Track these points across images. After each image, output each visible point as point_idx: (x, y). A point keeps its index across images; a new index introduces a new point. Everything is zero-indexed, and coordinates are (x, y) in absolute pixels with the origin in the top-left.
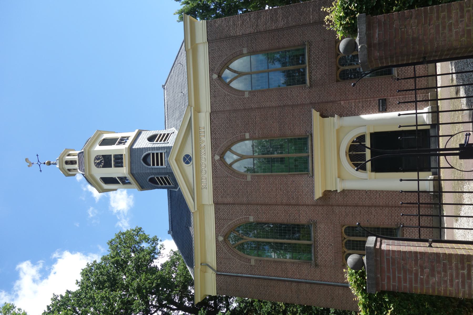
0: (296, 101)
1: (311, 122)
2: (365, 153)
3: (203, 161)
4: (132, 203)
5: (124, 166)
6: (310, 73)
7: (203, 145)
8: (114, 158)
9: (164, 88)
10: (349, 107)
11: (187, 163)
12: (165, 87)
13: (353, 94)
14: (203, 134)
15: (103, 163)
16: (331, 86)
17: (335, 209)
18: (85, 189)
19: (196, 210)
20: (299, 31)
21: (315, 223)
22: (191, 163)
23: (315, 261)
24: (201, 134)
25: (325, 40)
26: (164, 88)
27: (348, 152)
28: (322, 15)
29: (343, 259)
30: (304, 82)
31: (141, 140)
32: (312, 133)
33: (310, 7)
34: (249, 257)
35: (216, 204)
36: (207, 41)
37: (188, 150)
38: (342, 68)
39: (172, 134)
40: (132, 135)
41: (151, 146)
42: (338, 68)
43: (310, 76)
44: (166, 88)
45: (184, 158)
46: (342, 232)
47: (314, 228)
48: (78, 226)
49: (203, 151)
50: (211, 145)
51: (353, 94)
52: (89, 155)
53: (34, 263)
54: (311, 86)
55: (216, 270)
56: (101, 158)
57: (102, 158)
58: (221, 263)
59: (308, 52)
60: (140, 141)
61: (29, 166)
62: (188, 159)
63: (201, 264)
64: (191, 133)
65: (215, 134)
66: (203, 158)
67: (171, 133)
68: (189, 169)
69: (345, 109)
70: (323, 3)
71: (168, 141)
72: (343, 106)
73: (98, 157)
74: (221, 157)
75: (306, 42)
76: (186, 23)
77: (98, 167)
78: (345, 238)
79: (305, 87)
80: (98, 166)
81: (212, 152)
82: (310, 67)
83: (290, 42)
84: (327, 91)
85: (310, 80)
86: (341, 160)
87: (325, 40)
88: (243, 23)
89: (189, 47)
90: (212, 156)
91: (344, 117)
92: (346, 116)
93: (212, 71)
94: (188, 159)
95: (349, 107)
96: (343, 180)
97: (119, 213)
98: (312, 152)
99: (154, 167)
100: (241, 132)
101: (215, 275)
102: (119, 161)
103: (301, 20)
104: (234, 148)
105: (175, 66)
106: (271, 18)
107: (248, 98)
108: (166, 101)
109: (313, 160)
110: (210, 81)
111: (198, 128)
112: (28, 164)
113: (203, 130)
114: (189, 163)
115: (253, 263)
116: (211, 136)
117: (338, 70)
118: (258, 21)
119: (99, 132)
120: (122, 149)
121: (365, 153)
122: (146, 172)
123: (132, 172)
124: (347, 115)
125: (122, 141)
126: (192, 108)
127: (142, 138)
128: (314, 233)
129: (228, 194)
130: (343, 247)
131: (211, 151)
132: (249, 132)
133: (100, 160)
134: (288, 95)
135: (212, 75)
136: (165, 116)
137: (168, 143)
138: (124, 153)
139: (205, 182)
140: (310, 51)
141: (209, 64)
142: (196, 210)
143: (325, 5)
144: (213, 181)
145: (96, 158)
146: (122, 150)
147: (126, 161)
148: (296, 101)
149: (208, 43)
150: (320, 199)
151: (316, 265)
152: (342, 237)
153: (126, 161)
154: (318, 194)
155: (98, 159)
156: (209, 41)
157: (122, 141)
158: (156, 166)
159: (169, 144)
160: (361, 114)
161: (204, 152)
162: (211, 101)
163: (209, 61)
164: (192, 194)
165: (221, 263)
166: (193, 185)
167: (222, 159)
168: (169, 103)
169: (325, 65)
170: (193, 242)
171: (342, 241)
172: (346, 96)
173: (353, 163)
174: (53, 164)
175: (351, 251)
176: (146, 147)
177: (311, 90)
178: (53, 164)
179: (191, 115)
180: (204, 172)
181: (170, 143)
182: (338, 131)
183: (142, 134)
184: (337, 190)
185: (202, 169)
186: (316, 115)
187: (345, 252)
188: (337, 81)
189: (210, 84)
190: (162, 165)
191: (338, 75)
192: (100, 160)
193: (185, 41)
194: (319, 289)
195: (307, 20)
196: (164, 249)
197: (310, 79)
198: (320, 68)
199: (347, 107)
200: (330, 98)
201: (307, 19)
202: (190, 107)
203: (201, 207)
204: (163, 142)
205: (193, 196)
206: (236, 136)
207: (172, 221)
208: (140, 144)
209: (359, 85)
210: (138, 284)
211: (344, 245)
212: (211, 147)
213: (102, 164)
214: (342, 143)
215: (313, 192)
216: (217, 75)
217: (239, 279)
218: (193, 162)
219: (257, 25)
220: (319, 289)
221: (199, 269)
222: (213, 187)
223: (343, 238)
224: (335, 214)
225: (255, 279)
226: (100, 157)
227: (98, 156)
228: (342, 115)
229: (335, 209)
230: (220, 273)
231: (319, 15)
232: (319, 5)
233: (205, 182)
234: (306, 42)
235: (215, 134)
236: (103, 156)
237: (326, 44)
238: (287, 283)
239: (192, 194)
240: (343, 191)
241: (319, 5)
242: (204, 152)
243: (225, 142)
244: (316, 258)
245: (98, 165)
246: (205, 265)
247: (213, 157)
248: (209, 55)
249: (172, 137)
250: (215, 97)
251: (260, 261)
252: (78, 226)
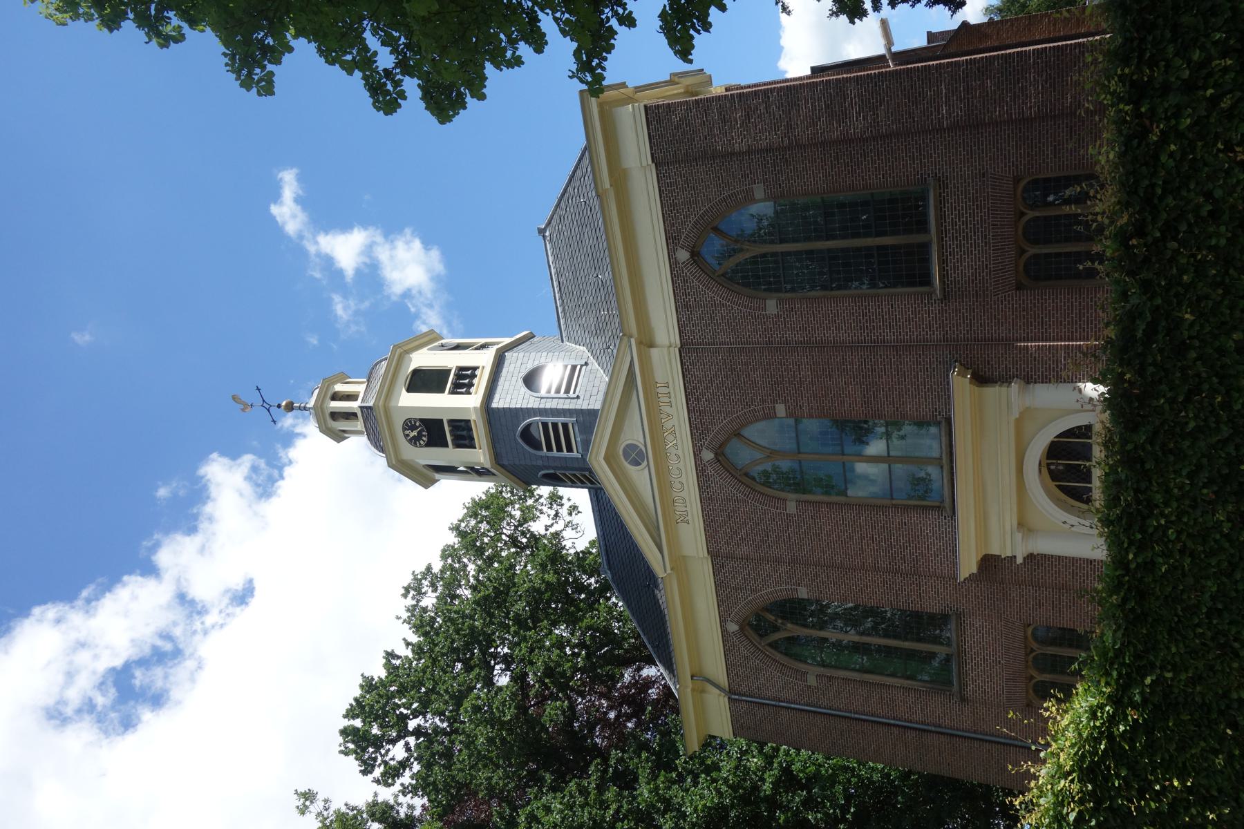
0: (907, 332)
1: (948, 389)
2: (1089, 485)
3: (672, 460)
4: (440, 268)
5: (477, 446)
6: (942, 262)
7: (668, 425)
8: (451, 435)
9: (544, 237)
10: (1050, 359)
11: (636, 463)
12: (547, 234)
13: (1061, 325)
14: (667, 400)
15: (425, 436)
16: (1002, 301)
17: (1010, 590)
18: (312, 249)
19: (669, 571)
20: (909, 144)
21: (959, 616)
22: (645, 463)
23: (961, 692)
24: (660, 390)
25: (984, 174)
26: (544, 237)
27: (1045, 462)
28: (976, 106)
29: (1027, 692)
30: (926, 280)
31: (507, 383)
32: (950, 415)
33: (941, 81)
34: (802, 667)
35: (716, 556)
36: (653, 161)
37: (635, 434)
38: (1032, 251)
39: (584, 368)
40: (483, 360)
41: (536, 406)
42: (1023, 251)
43: (942, 269)
44: (548, 238)
45: (624, 450)
46: (1026, 638)
47: (957, 626)
48: (315, 342)
49: (671, 438)
50: (691, 427)
51: (1061, 325)
52: (394, 445)
53: (233, 454)
54: (946, 296)
55: (727, 689)
56: (418, 424)
57: (420, 426)
58: (737, 675)
59: (936, 207)
60: (506, 387)
61: (243, 410)
62: (635, 456)
63: (692, 677)
64: (635, 393)
65: (698, 400)
66: (673, 454)
67: (582, 366)
68: (641, 477)
69: (1039, 364)
70: (979, 72)
71: (577, 393)
72: (1035, 357)
73: (410, 422)
74: (716, 454)
75: (929, 176)
76: (590, 126)
77: (415, 445)
78: (1032, 650)
79: (930, 294)
80: (415, 444)
81: (693, 442)
82: (941, 247)
83: (883, 175)
84: (991, 312)
85: (944, 282)
86: (1027, 487)
87: (984, 174)
88: (748, 116)
89: (607, 185)
90: (694, 452)
91: (1035, 383)
92: (1043, 383)
93: (672, 239)
94: (635, 456)
95: (1050, 359)
96: (1030, 530)
97: (407, 294)
98: (951, 461)
99: (550, 454)
100: (763, 401)
101: (726, 699)
102: (462, 433)
103: (914, 118)
104: (749, 432)
105: (567, 195)
106: (827, 106)
107: (777, 316)
108: (553, 271)
109: (953, 480)
110: (670, 266)
111: (650, 385)
112: (242, 407)
113: (665, 390)
114: (640, 464)
115: (812, 681)
116: (687, 403)
117: (1020, 257)
118: (790, 114)
119: (399, 351)
120: (468, 403)
121: (1089, 485)
122: (534, 463)
123: (497, 457)
124: (1044, 380)
125: (464, 380)
126: (633, 341)
127: (510, 375)
128: (957, 636)
129: (742, 539)
130: (1027, 667)
131: (692, 439)
132: (785, 402)
133: (417, 431)
134: (883, 316)
135: (675, 251)
136: (549, 266)
137: (578, 397)
138: (473, 417)
139: (684, 509)
140: (940, 202)
141: (664, 222)
142: (669, 571)
143: (985, 77)
144: (702, 506)
145: (407, 425)
146: (466, 410)
147: (480, 433)
148: (907, 332)
149: (656, 165)
150: (971, 578)
151: (963, 700)
152: (1026, 647)
153: (480, 433)
154: (968, 566)
155: (413, 428)
156: (658, 162)
157: (464, 380)
158: (555, 453)
159: (580, 401)
160: (1084, 379)
161: (675, 442)
162: (678, 317)
163: (663, 214)
164: (655, 535)
165: (737, 675)
166: (655, 516)
167: (720, 459)
168: (563, 279)
169: (986, 242)
170: (667, 618)
171: (1027, 655)
172: (1042, 328)
173: (1057, 486)
174: (299, 408)
175: (1048, 676)
176: (524, 406)
177: (946, 306)
178: (299, 408)
179: (632, 357)
180: (677, 485)
181: (582, 397)
182: (1019, 423)
183: (507, 363)
184: (1015, 557)
185: (673, 479)
186: (960, 383)
187: (1032, 677)
188: (1019, 287)
189: (672, 274)
190: (570, 449)
191: (1021, 268)
192: (417, 431)
193: (588, 149)
194: (971, 748)
195: (932, 119)
196: (579, 512)
197: (942, 278)
198: (972, 251)
199: (1045, 359)
200: (999, 329)
201: (932, 115)
202: (625, 339)
203: (680, 564)
204: (565, 396)
205: (658, 541)
206: (752, 408)
207: (607, 551)
208: (509, 397)
209: (1080, 302)
210: (545, 662)
211: (1030, 663)
212: (691, 430)
213: (424, 438)
214: (1031, 445)
215: (955, 565)
216: (689, 254)
217: (784, 712)
218: (648, 461)
219: (789, 126)
220: (971, 748)
221: (689, 690)
222: (704, 521)
223: (1029, 650)
224: (1010, 600)
225: (819, 716)
226: (415, 422)
227: (409, 420)
228: (1032, 378)
229: (1010, 590)
230: (737, 697)
231: (968, 105)
232: (967, 77)
233: (684, 509)
234: (929, 176)
235: (698, 400)
236: (424, 422)
237: (988, 193)
238: (896, 731)
239: (655, 535)
240: (1030, 557)
241: (967, 77)
242: (675, 442)
243: (724, 422)
244: (962, 686)
245: (414, 441)
246: (699, 677)
247: (671, 257)
248: (661, 197)
249: (586, 380)
250: (687, 307)
251: (830, 678)
252: (315, 342)
